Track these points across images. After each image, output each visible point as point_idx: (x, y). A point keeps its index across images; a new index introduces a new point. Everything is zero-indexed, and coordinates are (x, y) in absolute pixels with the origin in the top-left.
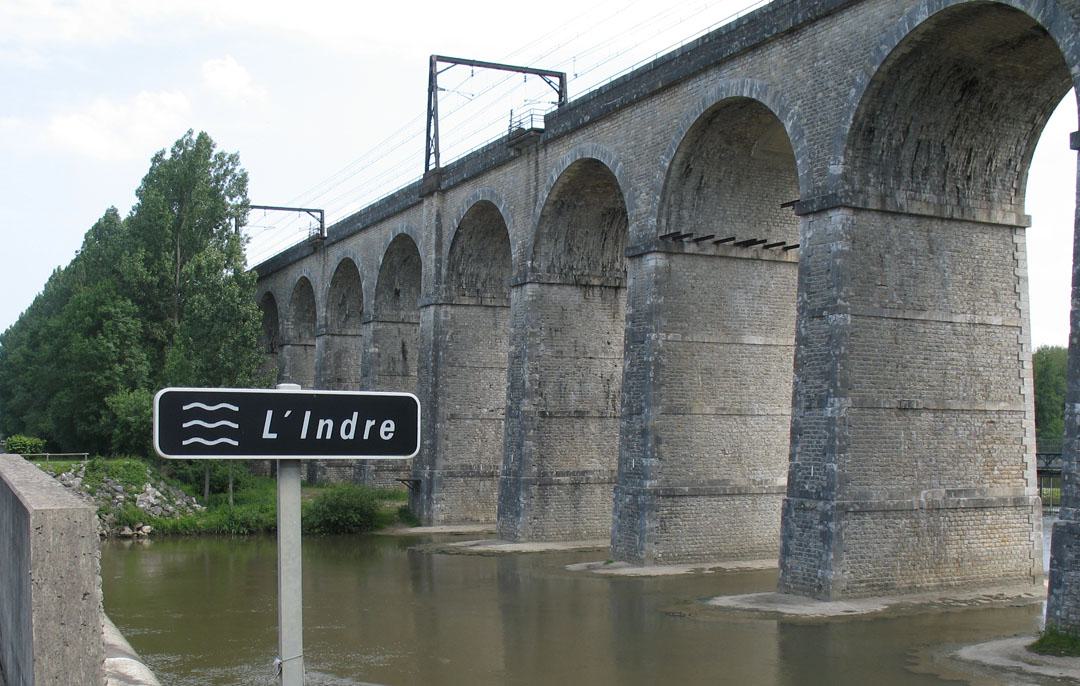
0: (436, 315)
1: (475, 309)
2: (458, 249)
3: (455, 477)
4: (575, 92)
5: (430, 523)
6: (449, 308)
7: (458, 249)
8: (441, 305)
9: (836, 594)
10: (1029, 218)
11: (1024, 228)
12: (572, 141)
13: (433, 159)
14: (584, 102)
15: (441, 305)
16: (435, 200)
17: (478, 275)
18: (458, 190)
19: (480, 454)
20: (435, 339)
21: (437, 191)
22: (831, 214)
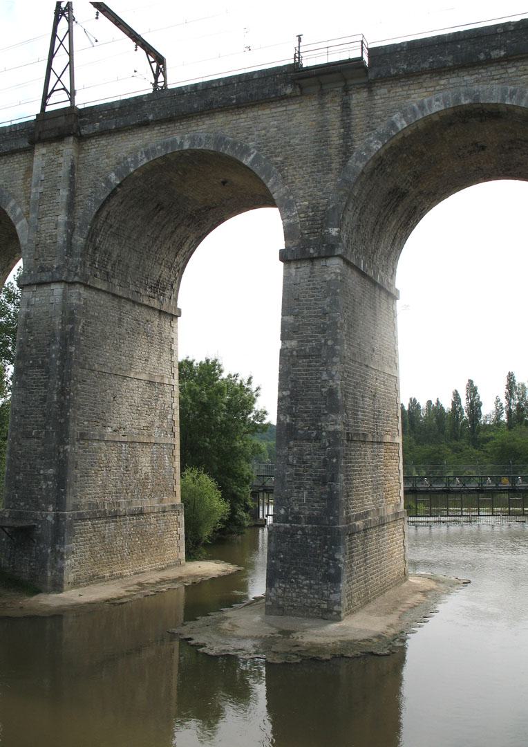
0: (65, 296)
1: (104, 296)
2: (105, 214)
3: (84, 520)
4: (178, 77)
5: (58, 587)
6: (82, 290)
7: (105, 214)
8: (73, 283)
9: (65, 586)
10: (179, 311)
11: (177, 317)
12: (442, 82)
13: (161, 78)
14: (92, 112)
15: (73, 283)
16: (68, 148)
17: (110, 253)
18: (112, 140)
19: (104, 486)
20: (63, 329)
21: (74, 135)
22: (53, 286)
